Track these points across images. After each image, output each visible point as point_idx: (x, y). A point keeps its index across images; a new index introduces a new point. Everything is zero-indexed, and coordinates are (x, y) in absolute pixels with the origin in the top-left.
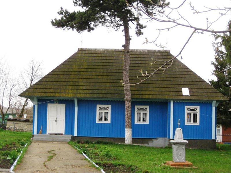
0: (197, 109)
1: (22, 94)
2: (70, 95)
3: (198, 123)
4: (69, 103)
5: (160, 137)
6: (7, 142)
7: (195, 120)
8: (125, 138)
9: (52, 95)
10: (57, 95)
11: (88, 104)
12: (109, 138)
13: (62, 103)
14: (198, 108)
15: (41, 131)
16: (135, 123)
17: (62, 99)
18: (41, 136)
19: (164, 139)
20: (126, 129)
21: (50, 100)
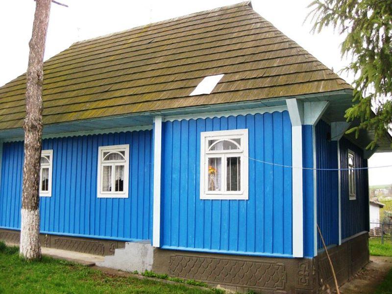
0: (238, 141)
3: (243, 193)
6: (211, 188)
7: (233, 184)
12: (48, 234)
14: (243, 134)
16: (99, 196)
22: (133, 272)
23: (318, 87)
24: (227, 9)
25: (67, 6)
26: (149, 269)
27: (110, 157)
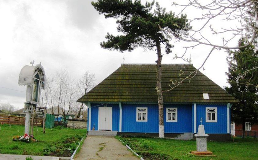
2: (116, 100)
3: (216, 121)
4: (115, 107)
7: (214, 119)
8: (158, 133)
9: (102, 100)
10: (106, 100)
15: (93, 128)
17: (109, 103)
20: (160, 126)
22: (189, 140)
23: (101, 100)
24: (153, 66)
25: (222, 28)
26: (192, 139)
27: (140, 110)
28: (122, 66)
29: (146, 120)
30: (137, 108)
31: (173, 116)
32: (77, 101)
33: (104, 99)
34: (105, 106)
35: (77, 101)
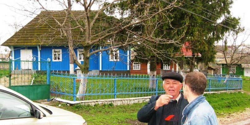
1: (3, 44)
2: (34, 44)
4: (34, 49)
5: (94, 69)
8: (69, 71)
9: (23, 44)
10: (26, 44)
11: (47, 49)
13: (30, 49)
15: (17, 68)
17: (29, 46)
18: (16, 71)
19: (96, 70)
20: (70, 65)
21: (20, 47)
28: (41, 12)
29: (61, 60)
30: (53, 50)
31: (58, 56)
32: (1, 45)
33: (24, 42)
34: (26, 49)
35: (1, 45)
